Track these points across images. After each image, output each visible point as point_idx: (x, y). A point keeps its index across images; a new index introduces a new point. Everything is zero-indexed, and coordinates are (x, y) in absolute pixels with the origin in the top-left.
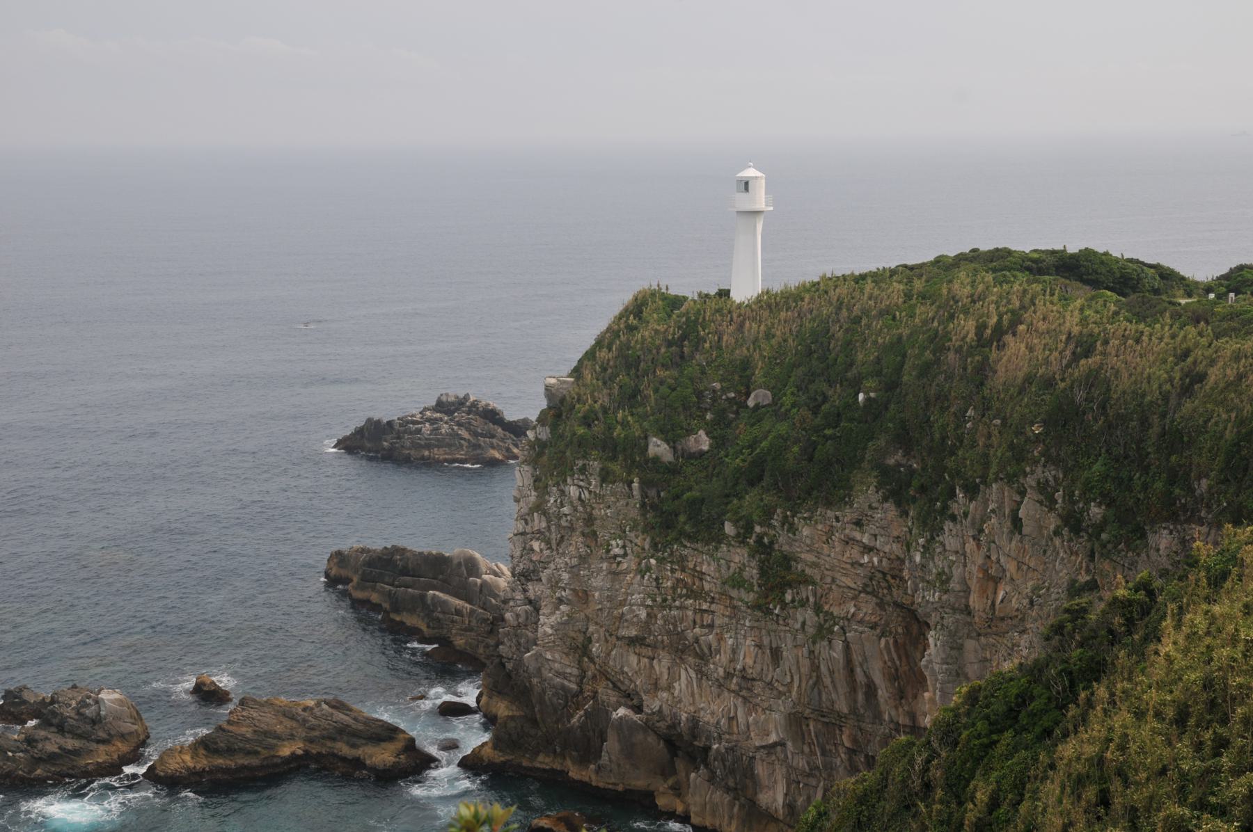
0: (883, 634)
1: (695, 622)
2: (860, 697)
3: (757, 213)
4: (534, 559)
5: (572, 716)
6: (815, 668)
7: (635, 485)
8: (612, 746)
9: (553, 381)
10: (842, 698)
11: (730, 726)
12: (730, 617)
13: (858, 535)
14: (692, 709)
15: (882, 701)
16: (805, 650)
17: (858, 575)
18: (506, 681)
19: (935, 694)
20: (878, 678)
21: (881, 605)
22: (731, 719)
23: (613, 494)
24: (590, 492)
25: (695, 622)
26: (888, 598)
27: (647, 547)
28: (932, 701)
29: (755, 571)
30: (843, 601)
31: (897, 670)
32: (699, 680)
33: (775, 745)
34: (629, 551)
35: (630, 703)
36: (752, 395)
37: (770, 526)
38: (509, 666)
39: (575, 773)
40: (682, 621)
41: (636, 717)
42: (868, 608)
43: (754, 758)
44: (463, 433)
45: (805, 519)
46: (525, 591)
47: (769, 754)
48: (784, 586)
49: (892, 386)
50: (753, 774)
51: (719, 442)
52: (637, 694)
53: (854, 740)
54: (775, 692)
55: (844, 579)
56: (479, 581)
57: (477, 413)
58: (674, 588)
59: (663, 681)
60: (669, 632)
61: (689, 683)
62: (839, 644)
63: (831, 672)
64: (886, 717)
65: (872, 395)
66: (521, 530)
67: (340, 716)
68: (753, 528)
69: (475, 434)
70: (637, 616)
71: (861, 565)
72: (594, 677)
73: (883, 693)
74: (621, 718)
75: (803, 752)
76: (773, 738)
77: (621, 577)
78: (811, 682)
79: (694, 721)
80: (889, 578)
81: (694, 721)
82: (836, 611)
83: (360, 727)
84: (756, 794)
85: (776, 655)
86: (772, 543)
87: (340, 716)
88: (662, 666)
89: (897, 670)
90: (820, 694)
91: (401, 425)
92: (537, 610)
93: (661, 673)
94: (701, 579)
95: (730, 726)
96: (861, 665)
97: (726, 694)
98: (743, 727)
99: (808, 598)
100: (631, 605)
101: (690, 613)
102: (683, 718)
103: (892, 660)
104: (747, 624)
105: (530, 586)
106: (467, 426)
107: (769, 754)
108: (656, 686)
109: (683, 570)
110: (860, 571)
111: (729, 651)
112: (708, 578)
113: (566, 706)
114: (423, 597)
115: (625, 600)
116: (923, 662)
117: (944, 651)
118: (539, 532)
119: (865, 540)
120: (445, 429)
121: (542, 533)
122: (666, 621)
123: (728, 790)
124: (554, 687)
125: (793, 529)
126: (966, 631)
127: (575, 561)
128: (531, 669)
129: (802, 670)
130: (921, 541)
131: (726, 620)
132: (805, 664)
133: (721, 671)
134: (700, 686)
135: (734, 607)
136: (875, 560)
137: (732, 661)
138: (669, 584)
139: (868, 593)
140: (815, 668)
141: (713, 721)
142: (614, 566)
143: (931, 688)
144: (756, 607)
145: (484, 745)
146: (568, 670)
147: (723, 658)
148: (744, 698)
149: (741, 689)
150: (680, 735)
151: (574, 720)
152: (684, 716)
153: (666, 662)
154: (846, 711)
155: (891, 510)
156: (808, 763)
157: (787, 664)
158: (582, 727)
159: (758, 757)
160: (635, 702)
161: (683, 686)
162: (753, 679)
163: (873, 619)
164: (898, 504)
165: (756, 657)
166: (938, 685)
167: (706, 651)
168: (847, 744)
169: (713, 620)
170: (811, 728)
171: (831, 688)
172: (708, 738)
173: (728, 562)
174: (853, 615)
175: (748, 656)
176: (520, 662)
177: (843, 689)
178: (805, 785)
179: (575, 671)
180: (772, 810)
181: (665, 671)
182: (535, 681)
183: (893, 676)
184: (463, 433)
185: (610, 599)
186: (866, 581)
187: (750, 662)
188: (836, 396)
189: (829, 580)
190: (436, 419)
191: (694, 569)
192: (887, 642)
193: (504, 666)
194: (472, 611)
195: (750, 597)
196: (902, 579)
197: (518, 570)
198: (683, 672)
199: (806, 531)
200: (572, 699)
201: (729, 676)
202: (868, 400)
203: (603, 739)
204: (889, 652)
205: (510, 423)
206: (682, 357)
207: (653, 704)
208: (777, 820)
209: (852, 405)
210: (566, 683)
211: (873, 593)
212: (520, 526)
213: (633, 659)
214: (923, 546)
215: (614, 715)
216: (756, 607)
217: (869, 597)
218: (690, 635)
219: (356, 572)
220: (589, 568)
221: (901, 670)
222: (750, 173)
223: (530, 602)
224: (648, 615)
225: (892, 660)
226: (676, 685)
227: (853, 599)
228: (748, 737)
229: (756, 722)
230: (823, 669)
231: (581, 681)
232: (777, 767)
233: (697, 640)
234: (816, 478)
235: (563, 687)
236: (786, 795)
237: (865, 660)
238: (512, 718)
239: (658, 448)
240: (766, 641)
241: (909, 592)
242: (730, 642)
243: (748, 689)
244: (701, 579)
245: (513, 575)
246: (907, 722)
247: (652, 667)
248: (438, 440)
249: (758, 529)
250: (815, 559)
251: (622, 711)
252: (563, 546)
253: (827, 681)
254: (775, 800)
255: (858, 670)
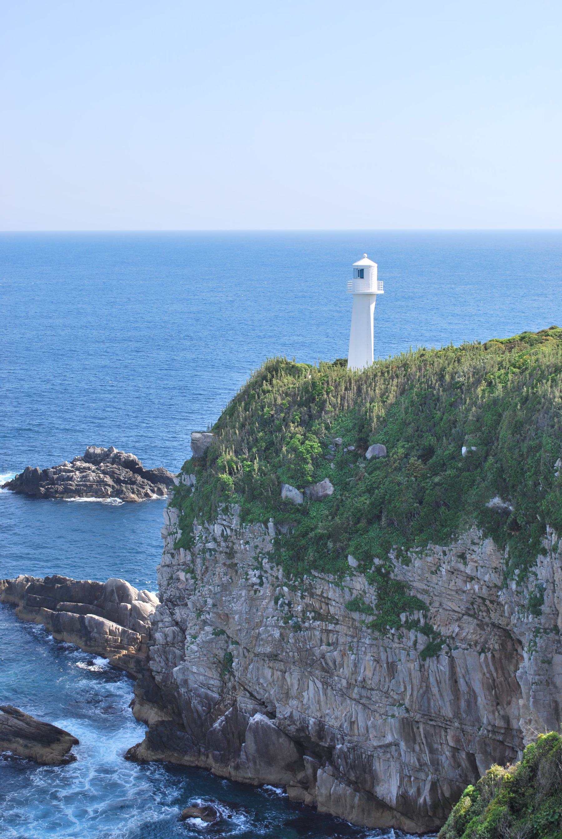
0: (483, 651)
1: (321, 640)
2: (463, 704)
3: (370, 295)
4: (180, 587)
5: (214, 721)
6: (425, 679)
7: (271, 524)
8: (250, 744)
9: (198, 435)
10: (448, 704)
11: (352, 729)
12: (353, 637)
13: (461, 567)
14: (319, 715)
15: (481, 707)
16: (417, 664)
17: (461, 600)
18: (155, 692)
19: (528, 700)
20: (477, 687)
21: (481, 626)
22: (352, 723)
23: (252, 532)
24: (232, 530)
25: (321, 640)
26: (487, 620)
27: (280, 577)
28: (526, 707)
29: (374, 597)
30: (447, 624)
31: (494, 680)
32: (325, 691)
33: (389, 745)
34: (264, 580)
35: (264, 710)
36: (370, 449)
37: (387, 559)
38: (158, 678)
39: (217, 769)
40: (310, 639)
41: (270, 722)
42: (469, 629)
43: (372, 756)
44: (108, 480)
45: (416, 553)
46: (172, 614)
47: (385, 752)
48: (397, 609)
49: (487, 442)
50: (371, 770)
51: (342, 486)
52: (271, 702)
53: (457, 740)
54: (390, 700)
55: (450, 604)
56: (129, 606)
57: (119, 464)
58: (304, 612)
59: (294, 692)
60: (299, 650)
61: (317, 692)
62: (445, 660)
63: (438, 683)
64: (485, 721)
65: (474, 448)
66: (167, 563)
67: (14, 721)
68: (372, 560)
69: (118, 481)
70: (271, 635)
71: (464, 592)
72: (234, 688)
73: (481, 701)
74: (257, 723)
75: (414, 751)
76: (389, 739)
77: (258, 602)
78: (421, 691)
79: (321, 727)
80: (488, 602)
81: (321, 727)
82: (444, 631)
83: (33, 730)
84: (373, 786)
85: (392, 669)
86: (388, 573)
87: (14, 721)
88: (292, 680)
89: (494, 680)
90: (429, 700)
91: (55, 473)
92: (183, 631)
93: (292, 685)
94: (327, 604)
95: (352, 729)
96: (464, 677)
97: (349, 702)
98: (362, 730)
99: (419, 621)
100: (266, 626)
101: (317, 633)
102: (311, 722)
103: (490, 672)
104: (367, 642)
105: (177, 610)
106: (112, 475)
107: (385, 752)
108: (287, 695)
109: (312, 595)
110: (464, 597)
111: (351, 665)
112: (334, 603)
113: (209, 712)
114: (82, 619)
115: (261, 622)
116: (518, 673)
117: (536, 664)
118: (184, 564)
119: (468, 571)
120: (92, 476)
121: (188, 565)
122: (297, 640)
123: (349, 783)
124: (199, 696)
125: (407, 562)
126: (555, 647)
127: (218, 589)
128: (179, 681)
129: (414, 681)
130: (517, 571)
131: (349, 639)
132: (416, 675)
133: (344, 682)
134: (325, 694)
135: (356, 628)
136: (476, 587)
137: (355, 672)
138: (300, 608)
139: (470, 615)
140: (425, 679)
141: (337, 724)
142: (252, 592)
143: (524, 695)
144: (374, 626)
145: (138, 745)
146: (212, 682)
147: (346, 671)
148: (364, 705)
149: (361, 697)
150: (308, 738)
151: (216, 725)
152: (312, 721)
153: (296, 675)
154: (450, 715)
155: (489, 545)
156: (419, 760)
157: (401, 676)
158: (224, 729)
159: (375, 755)
160: (269, 709)
161: (311, 695)
162: (372, 689)
163: (474, 637)
164: (496, 540)
165: (375, 670)
166: (531, 693)
167: (331, 664)
168: (451, 744)
169: (337, 639)
170: (421, 730)
171: (438, 696)
172: (332, 740)
173: (351, 590)
174: (457, 635)
175: (367, 669)
176: (168, 676)
177: (448, 696)
178: (416, 778)
179: (217, 683)
180: (387, 800)
181: (296, 683)
182: (182, 690)
183: (492, 686)
184: (108, 480)
185: (248, 621)
186: (468, 605)
187: (369, 674)
188: (444, 450)
189: (437, 604)
190: (84, 468)
191: (321, 596)
192: (486, 657)
193: (154, 678)
194: (123, 631)
195: (370, 619)
196: (499, 604)
197: (165, 597)
198: (311, 683)
199: (417, 563)
200: (212, 708)
201: (350, 686)
202: (469, 452)
203: (242, 740)
204: (487, 666)
205: (148, 472)
206: (310, 416)
207: (283, 711)
208: (390, 808)
209: (455, 456)
210: (209, 692)
211: (473, 616)
212: (167, 559)
213: (268, 673)
214: (518, 576)
215: (251, 721)
216: (374, 626)
217: (471, 619)
218: (317, 651)
219: (22, 597)
220: (230, 594)
221: (497, 681)
222: (364, 262)
223: (177, 624)
224: (281, 634)
225: (490, 672)
226: (305, 694)
227: (457, 620)
228: (368, 739)
229: (374, 726)
230: (432, 680)
231: (222, 691)
232: (392, 764)
233: (323, 657)
234: (432, 519)
235: (207, 696)
236: (399, 787)
237: (467, 671)
238: (162, 722)
239: (290, 492)
240: (383, 657)
241: (506, 614)
242: (353, 657)
243: (367, 697)
244: (327, 604)
245: (161, 600)
246: (502, 724)
247: (284, 678)
248: (85, 486)
249: (377, 561)
250: (425, 587)
251: (258, 717)
252: (207, 575)
253: (435, 690)
254: (390, 792)
255: (461, 681)
